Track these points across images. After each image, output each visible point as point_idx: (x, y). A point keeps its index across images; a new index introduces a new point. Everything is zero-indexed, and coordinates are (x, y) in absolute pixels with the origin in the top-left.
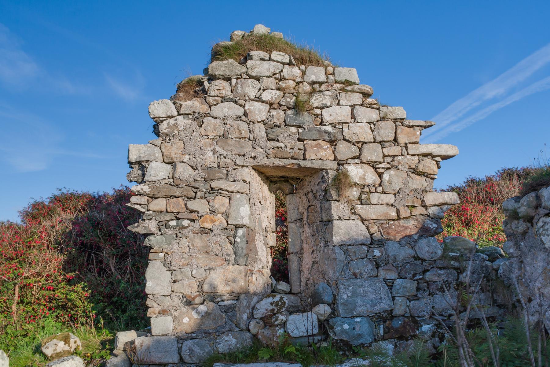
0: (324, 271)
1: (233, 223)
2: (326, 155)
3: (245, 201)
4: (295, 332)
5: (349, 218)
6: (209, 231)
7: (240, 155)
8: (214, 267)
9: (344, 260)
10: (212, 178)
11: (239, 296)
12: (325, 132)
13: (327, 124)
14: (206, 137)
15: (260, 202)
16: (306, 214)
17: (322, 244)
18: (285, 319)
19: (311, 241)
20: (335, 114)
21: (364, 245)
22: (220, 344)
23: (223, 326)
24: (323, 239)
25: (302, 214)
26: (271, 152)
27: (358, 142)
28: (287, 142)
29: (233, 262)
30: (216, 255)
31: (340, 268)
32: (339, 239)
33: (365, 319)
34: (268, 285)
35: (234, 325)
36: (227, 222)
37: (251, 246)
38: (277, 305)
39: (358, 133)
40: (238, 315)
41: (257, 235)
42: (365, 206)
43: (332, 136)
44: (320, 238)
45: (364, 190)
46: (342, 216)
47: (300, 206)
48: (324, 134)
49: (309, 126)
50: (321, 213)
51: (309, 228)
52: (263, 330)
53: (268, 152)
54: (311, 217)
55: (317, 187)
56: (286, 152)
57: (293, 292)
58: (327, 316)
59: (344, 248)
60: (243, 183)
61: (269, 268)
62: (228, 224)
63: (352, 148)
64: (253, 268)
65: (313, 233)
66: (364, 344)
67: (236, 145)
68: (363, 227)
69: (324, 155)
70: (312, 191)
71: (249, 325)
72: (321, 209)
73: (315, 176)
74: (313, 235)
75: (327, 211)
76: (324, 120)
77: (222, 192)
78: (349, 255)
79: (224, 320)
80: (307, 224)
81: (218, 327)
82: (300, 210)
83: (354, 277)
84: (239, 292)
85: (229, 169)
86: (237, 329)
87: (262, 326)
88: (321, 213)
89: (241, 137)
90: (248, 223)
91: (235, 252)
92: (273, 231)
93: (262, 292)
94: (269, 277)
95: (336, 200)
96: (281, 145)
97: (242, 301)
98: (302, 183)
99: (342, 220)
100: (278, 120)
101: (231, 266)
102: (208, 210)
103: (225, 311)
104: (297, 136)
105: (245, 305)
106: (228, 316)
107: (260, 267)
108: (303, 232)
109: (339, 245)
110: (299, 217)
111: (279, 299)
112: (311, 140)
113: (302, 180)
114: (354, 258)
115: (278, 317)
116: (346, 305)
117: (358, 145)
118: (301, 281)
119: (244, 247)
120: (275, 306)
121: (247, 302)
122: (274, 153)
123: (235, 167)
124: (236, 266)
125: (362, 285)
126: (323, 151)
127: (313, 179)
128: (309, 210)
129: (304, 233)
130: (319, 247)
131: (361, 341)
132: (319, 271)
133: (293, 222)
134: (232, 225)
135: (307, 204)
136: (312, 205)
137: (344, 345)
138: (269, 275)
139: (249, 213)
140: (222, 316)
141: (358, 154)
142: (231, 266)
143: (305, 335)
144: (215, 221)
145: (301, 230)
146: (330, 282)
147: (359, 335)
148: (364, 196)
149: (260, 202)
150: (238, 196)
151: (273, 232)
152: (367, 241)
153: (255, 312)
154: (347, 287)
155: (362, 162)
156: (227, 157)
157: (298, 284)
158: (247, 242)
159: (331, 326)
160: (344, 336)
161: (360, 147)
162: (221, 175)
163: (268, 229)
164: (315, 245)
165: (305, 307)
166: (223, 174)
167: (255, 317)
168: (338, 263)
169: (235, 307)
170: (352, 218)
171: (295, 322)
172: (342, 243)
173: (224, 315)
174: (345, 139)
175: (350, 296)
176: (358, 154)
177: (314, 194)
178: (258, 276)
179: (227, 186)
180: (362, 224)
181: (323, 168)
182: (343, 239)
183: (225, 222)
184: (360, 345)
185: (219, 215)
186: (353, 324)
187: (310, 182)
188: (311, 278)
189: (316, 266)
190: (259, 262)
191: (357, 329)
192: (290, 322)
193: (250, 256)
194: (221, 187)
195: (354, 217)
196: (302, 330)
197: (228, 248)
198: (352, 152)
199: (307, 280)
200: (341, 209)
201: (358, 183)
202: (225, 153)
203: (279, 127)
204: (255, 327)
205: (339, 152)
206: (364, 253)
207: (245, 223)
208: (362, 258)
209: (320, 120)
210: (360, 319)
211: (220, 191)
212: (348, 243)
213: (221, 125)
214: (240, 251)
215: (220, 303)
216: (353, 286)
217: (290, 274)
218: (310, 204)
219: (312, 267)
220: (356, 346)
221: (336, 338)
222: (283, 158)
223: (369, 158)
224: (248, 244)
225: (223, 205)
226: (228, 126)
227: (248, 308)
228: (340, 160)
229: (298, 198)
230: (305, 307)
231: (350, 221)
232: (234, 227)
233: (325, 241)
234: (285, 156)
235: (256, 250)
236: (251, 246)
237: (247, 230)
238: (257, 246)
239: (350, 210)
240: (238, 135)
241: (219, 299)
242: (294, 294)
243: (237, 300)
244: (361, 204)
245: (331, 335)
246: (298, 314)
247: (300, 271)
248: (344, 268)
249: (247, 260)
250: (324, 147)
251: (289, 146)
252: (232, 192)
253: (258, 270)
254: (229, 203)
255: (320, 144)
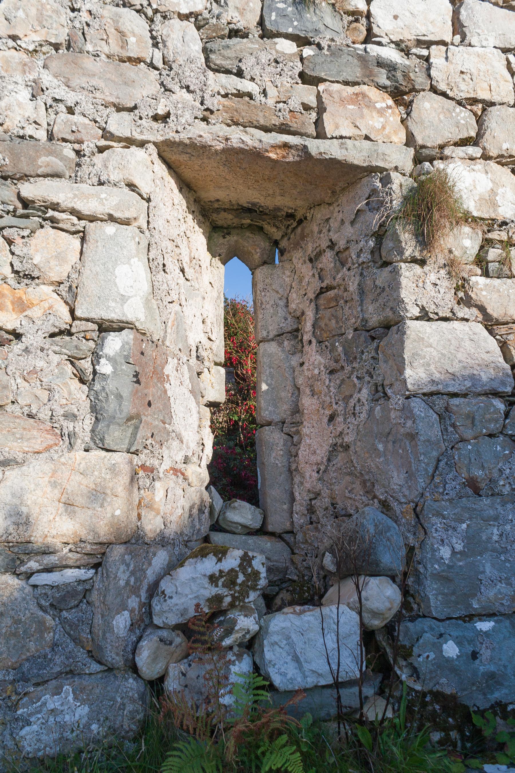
0: (369, 472)
1: (92, 315)
2: (384, 128)
3: (133, 245)
4: (292, 671)
5: (450, 315)
6: (11, 337)
7: (119, 109)
8: (20, 457)
9: (439, 441)
10: (27, 169)
11: (104, 554)
12: (380, 63)
13: (385, 40)
14: (11, 43)
15: (182, 271)
16: (310, 314)
17: (365, 395)
18: (256, 628)
19: (328, 387)
20: (408, 14)
21: (496, 394)
22: (29, 724)
23: (45, 656)
24: (367, 378)
25: (299, 318)
26: (219, 103)
27: (474, 101)
28: (267, 79)
29: (87, 439)
30: (30, 416)
31: (427, 464)
32: (423, 375)
33: (507, 623)
34: (201, 511)
35: (81, 655)
36: (72, 312)
37: (152, 392)
38: (231, 583)
39: (474, 71)
40: (98, 620)
41: (172, 362)
42: (497, 282)
43: (399, 75)
44: (358, 378)
45: (494, 235)
46: (431, 308)
47: (294, 295)
48: (377, 69)
49: (332, 40)
50: (361, 305)
51: (321, 352)
52: (183, 667)
53: (208, 103)
54: (326, 320)
55: (349, 231)
56: (263, 107)
57: (270, 528)
58: (390, 615)
59: (440, 403)
60: (126, 190)
61: (205, 462)
62: (74, 317)
63: (458, 115)
64: (156, 463)
65: (333, 365)
66: (506, 705)
67: (108, 76)
68: (492, 344)
69: (378, 126)
70: (332, 245)
71: (134, 652)
72: (362, 292)
73: (343, 199)
74: (332, 372)
75: (384, 294)
76: (376, 30)
77: (56, 214)
78: (454, 426)
79: (49, 637)
80: (314, 341)
81: (27, 660)
82: (293, 306)
83: (470, 491)
84: (103, 539)
85: (84, 146)
86: (95, 667)
87: (179, 651)
88: (361, 305)
89: (125, 54)
90: (142, 317)
91: (94, 409)
92: (218, 361)
93: (182, 534)
94: (203, 489)
95: (414, 260)
96: (246, 85)
97: (112, 569)
98: (299, 230)
99: (429, 320)
100: (242, 14)
101: (79, 454)
102: (7, 271)
103: (52, 605)
104: (299, 67)
105: (122, 583)
106: (64, 622)
107: (180, 458)
108: (302, 364)
109: (424, 394)
110: (289, 325)
111: (238, 561)
112: (338, 82)
113: (300, 222)
114: (468, 434)
115: (234, 622)
116: (448, 580)
117: (474, 108)
118: (293, 499)
119: (126, 393)
120: (224, 586)
121: (133, 573)
122: (227, 109)
123: (103, 143)
124: (97, 454)
125: (496, 518)
126: (375, 114)
127: (337, 209)
128: (322, 301)
129: (305, 367)
130: (352, 402)
131: (497, 695)
132: (350, 474)
133: (272, 340)
134: (87, 320)
135: (316, 285)
136: (329, 288)
137: (444, 708)
138: (206, 484)
139: (146, 287)
140: (41, 623)
141: (473, 134)
142: (79, 454)
143: (323, 683)
144: (31, 305)
145: (295, 361)
146: (395, 505)
147: (492, 676)
148: (493, 254)
149: (182, 271)
150: (111, 229)
151: (216, 364)
152: (503, 383)
153: (157, 608)
154: (453, 524)
155: (486, 157)
156: (77, 110)
157: (285, 507)
158: (136, 375)
159: (404, 647)
160: (444, 680)
161: (479, 113)
162: (59, 165)
163: (203, 354)
164: (341, 397)
165: (306, 572)
166: (63, 158)
167: (157, 621)
168: (421, 449)
169: (87, 591)
170: (460, 315)
171: (288, 638)
172: (434, 388)
173: (48, 617)
174: (434, 90)
175: (460, 553)
176: (473, 134)
177: (337, 254)
178: (172, 484)
179: (75, 196)
180: (486, 333)
181: (374, 164)
182: (437, 376)
183: (64, 311)
184: (492, 707)
185: (47, 290)
186: (471, 642)
187: (328, 220)
188: (326, 492)
189: (340, 459)
190: (175, 444)
191: (484, 658)
192: (275, 638)
193: (147, 423)
194: (55, 200)
195: (463, 312)
196: (314, 666)
197: (70, 393)
198: (457, 125)
199: (312, 496)
200: (429, 286)
201: (475, 214)
202: (71, 98)
203: (245, 36)
204: (155, 658)
205: (422, 123)
206: (496, 421)
207: (130, 317)
208: (490, 436)
209: (364, 30)
210: (492, 624)
211: (50, 213)
212: (451, 389)
213: (63, 10)
214: (112, 406)
215: (36, 579)
216: (470, 519)
217: (264, 479)
218: (324, 285)
219: (329, 460)
220: (481, 713)
221: (418, 687)
222: (256, 127)
223: (505, 146)
224: (138, 382)
225: (60, 257)
226: (85, 17)
227: (135, 591)
228: (423, 147)
229: (288, 273)
230: (306, 572)
231: (456, 324)
232: (96, 327)
233: (376, 385)
234: (262, 122)
235: (167, 406)
236: (152, 392)
237: (135, 339)
238: (169, 393)
239: (453, 291)
240: (114, 48)
241: (33, 565)
242: (272, 534)
243: (97, 566)
244: (486, 274)
245: (404, 677)
246: (298, 608)
247: (290, 471)
248: (442, 464)
249: (134, 435)
250: (378, 105)
251: (272, 92)
252: (92, 219)
253: (172, 469)
254: (81, 253)
255: (364, 95)
